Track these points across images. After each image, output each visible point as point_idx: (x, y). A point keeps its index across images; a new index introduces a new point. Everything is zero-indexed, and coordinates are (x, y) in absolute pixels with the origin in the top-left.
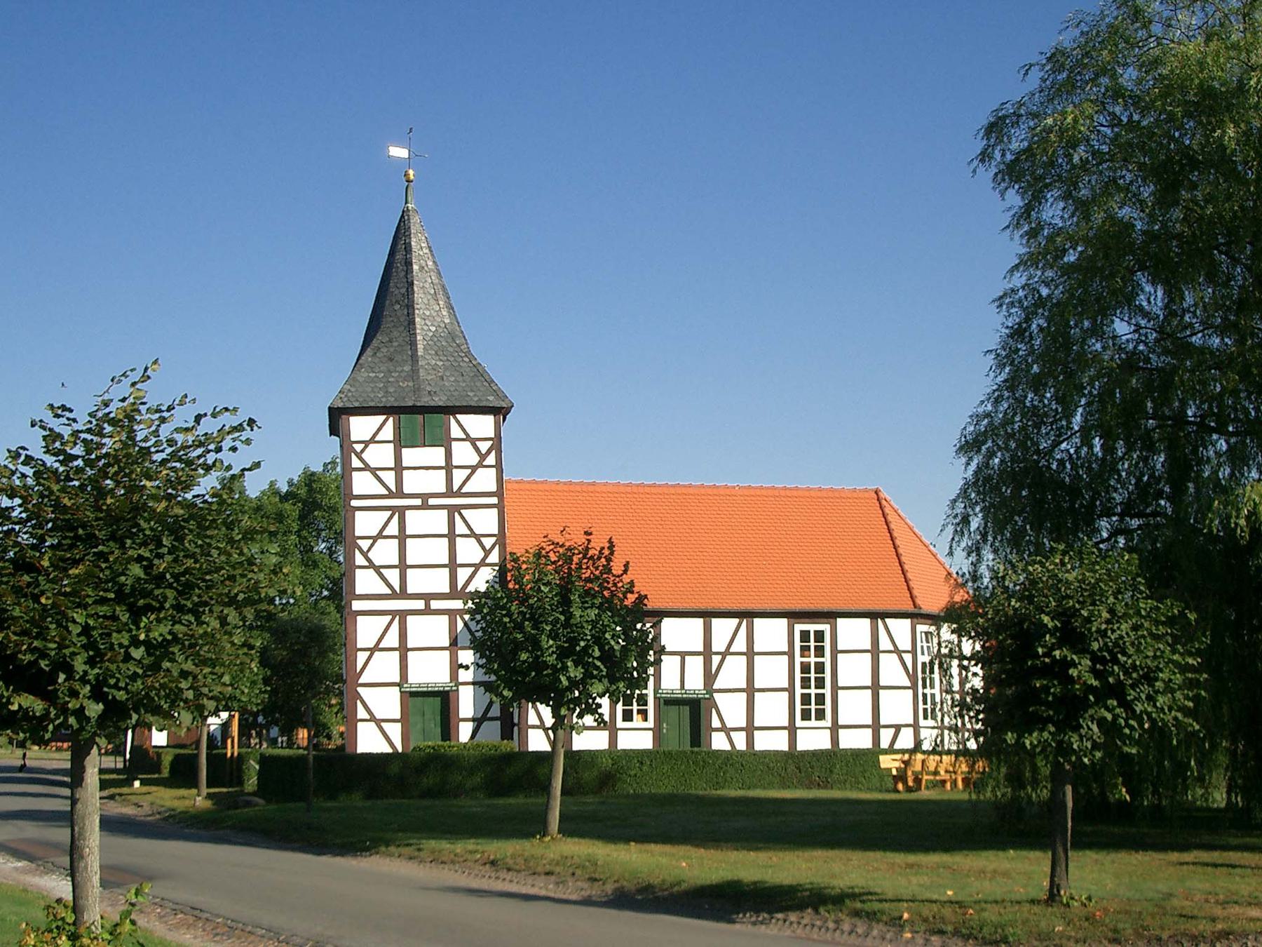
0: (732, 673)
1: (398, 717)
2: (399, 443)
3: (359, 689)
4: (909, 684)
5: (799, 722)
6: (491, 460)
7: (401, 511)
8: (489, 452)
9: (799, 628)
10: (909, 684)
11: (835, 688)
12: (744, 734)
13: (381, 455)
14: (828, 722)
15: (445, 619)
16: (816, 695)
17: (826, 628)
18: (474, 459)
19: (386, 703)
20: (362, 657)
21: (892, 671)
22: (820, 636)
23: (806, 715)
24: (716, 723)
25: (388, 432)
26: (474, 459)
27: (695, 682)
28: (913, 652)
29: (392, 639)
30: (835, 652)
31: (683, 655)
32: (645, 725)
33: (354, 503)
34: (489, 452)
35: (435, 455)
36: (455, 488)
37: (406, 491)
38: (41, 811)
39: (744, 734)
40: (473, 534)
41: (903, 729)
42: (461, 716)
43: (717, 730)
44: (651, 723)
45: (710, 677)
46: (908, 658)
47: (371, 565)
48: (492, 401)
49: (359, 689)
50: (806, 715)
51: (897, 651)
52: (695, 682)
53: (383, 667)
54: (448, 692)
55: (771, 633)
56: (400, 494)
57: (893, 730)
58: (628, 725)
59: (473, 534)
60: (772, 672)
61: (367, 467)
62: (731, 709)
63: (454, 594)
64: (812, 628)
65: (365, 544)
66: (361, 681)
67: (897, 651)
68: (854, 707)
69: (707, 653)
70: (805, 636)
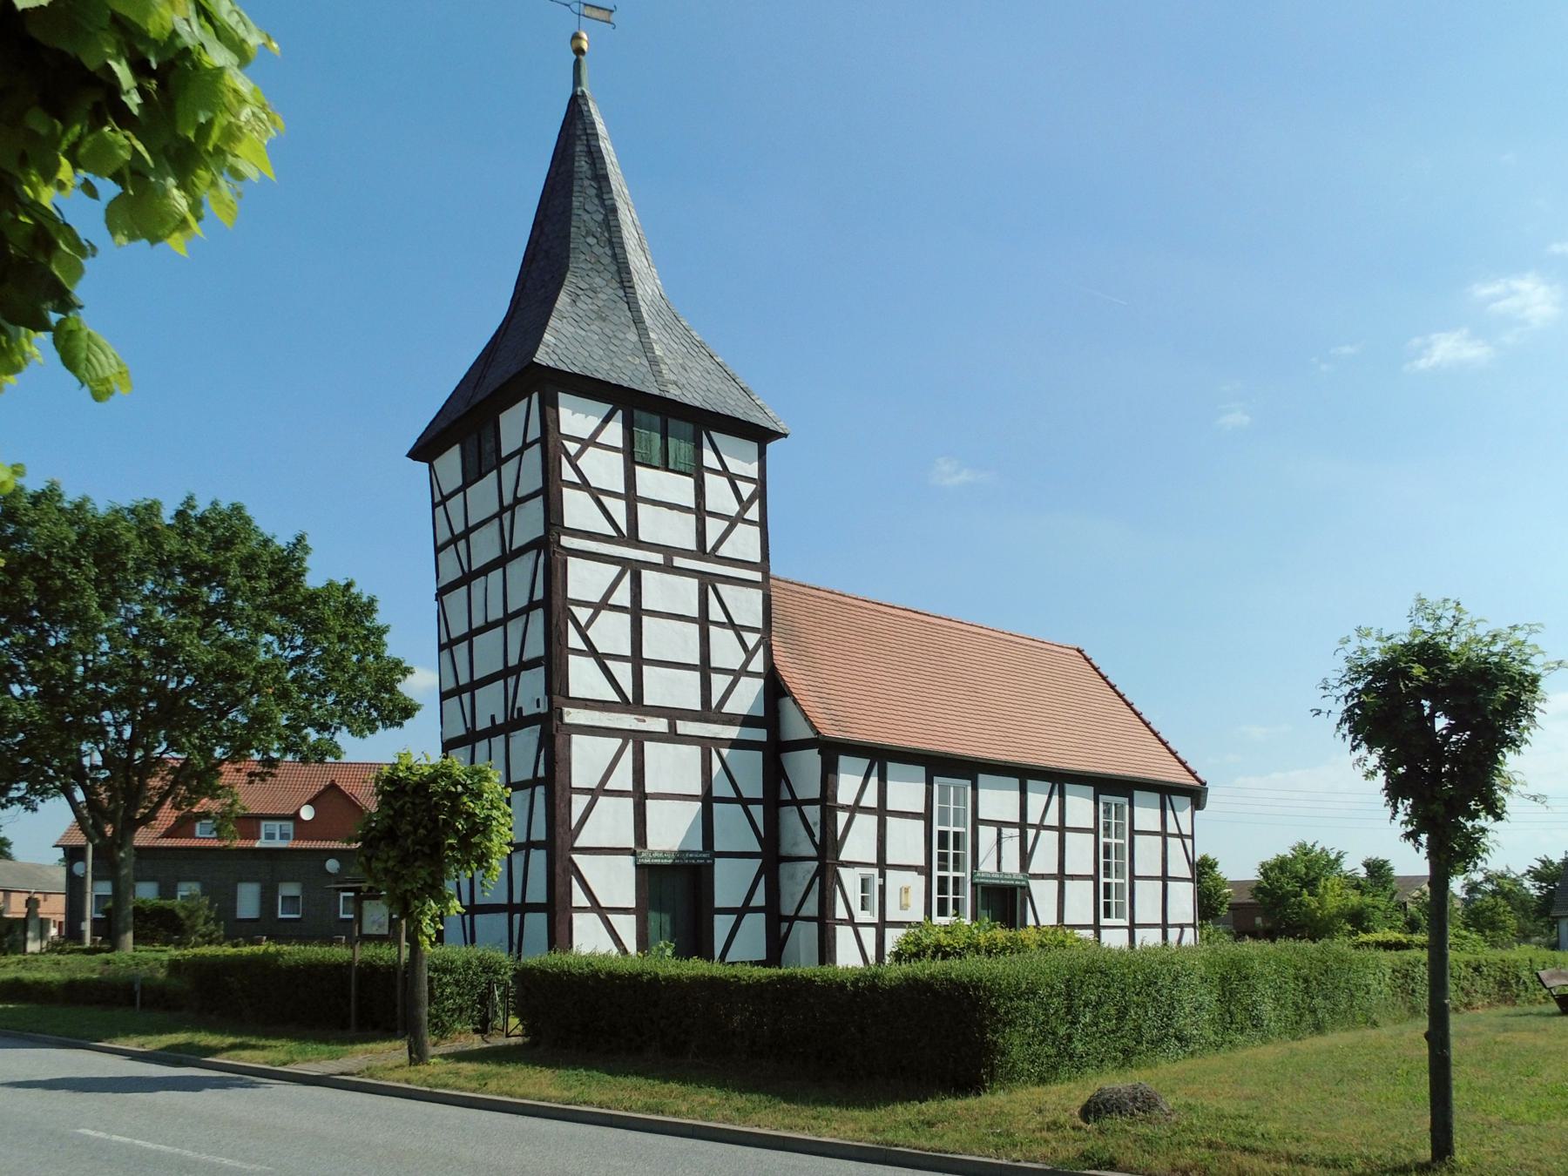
3: (576, 857)
6: (753, 513)
7: (634, 570)
8: (751, 500)
12: (873, 930)
13: (604, 468)
15: (695, 752)
18: (733, 508)
19: (613, 882)
20: (579, 803)
21: (611, 633)
27: (1011, 865)
29: (623, 778)
33: (566, 541)
34: (751, 500)
35: (680, 488)
37: (642, 537)
38: (115, 1091)
39: (873, 930)
40: (731, 624)
42: (718, 903)
45: (1025, 857)
47: (592, 651)
48: (1174, 774)
49: (576, 857)
53: (608, 823)
54: (699, 866)
56: (632, 539)
59: (731, 624)
61: (584, 485)
62: (1043, 895)
63: (709, 712)
65: (583, 614)
66: (756, 863)
69: (1023, 825)
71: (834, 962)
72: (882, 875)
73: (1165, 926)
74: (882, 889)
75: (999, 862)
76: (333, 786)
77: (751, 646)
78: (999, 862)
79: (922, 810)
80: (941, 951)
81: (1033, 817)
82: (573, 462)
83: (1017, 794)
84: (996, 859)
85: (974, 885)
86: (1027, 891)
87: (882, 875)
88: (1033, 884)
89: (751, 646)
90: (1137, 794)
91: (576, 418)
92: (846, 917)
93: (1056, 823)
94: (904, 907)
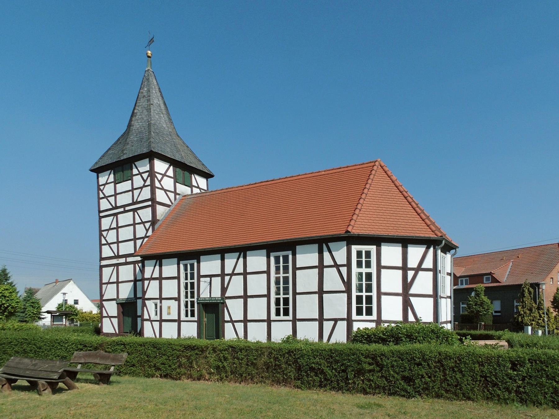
0: (236, 287)
1: (116, 315)
2: (116, 182)
4: (343, 289)
5: (354, 316)
6: (148, 182)
9: (355, 248)
10: (343, 289)
11: (295, 294)
14: (290, 317)
16: (366, 296)
17: (373, 249)
18: (141, 183)
22: (368, 254)
23: (359, 312)
24: (227, 318)
25: (112, 178)
26: (141, 183)
27: (217, 293)
28: (349, 265)
30: (295, 269)
31: (211, 276)
32: (193, 319)
36: (135, 201)
41: (339, 322)
43: (228, 322)
44: (196, 318)
45: (224, 290)
46: (344, 270)
50: (359, 312)
51: (337, 266)
52: (217, 293)
55: (257, 261)
57: (333, 322)
58: (278, 318)
60: (258, 284)
61: (162, 189)
64: (364, 248)
67: (337, 266)
68: (307, 307)
70: (359, 254)
71: (224, 336)
72: (161, 302)
73: (321, 320)
74: (161, 307)
75: (210, 293)
76: (538, 285)
77: (147, 228)
78: (210, 293)
79: (383, 270)
80: (410, 337)
81: (228, 270)
82: (160, 181)
83: (219, 262)
84: (209, 291)
85: (198, 303)
86: (224, 304)
87: (161, 302)
88: (228, 301)
89: (147, 228)
90: (298, 248)
91: (160, 166)
92: (148, 318)
93: (431, 266)
94: (169, 314)
